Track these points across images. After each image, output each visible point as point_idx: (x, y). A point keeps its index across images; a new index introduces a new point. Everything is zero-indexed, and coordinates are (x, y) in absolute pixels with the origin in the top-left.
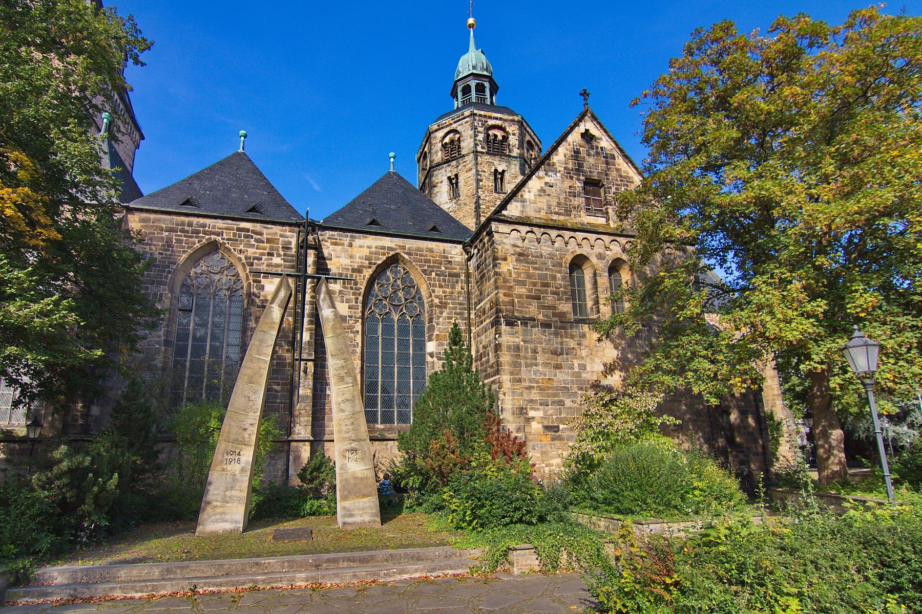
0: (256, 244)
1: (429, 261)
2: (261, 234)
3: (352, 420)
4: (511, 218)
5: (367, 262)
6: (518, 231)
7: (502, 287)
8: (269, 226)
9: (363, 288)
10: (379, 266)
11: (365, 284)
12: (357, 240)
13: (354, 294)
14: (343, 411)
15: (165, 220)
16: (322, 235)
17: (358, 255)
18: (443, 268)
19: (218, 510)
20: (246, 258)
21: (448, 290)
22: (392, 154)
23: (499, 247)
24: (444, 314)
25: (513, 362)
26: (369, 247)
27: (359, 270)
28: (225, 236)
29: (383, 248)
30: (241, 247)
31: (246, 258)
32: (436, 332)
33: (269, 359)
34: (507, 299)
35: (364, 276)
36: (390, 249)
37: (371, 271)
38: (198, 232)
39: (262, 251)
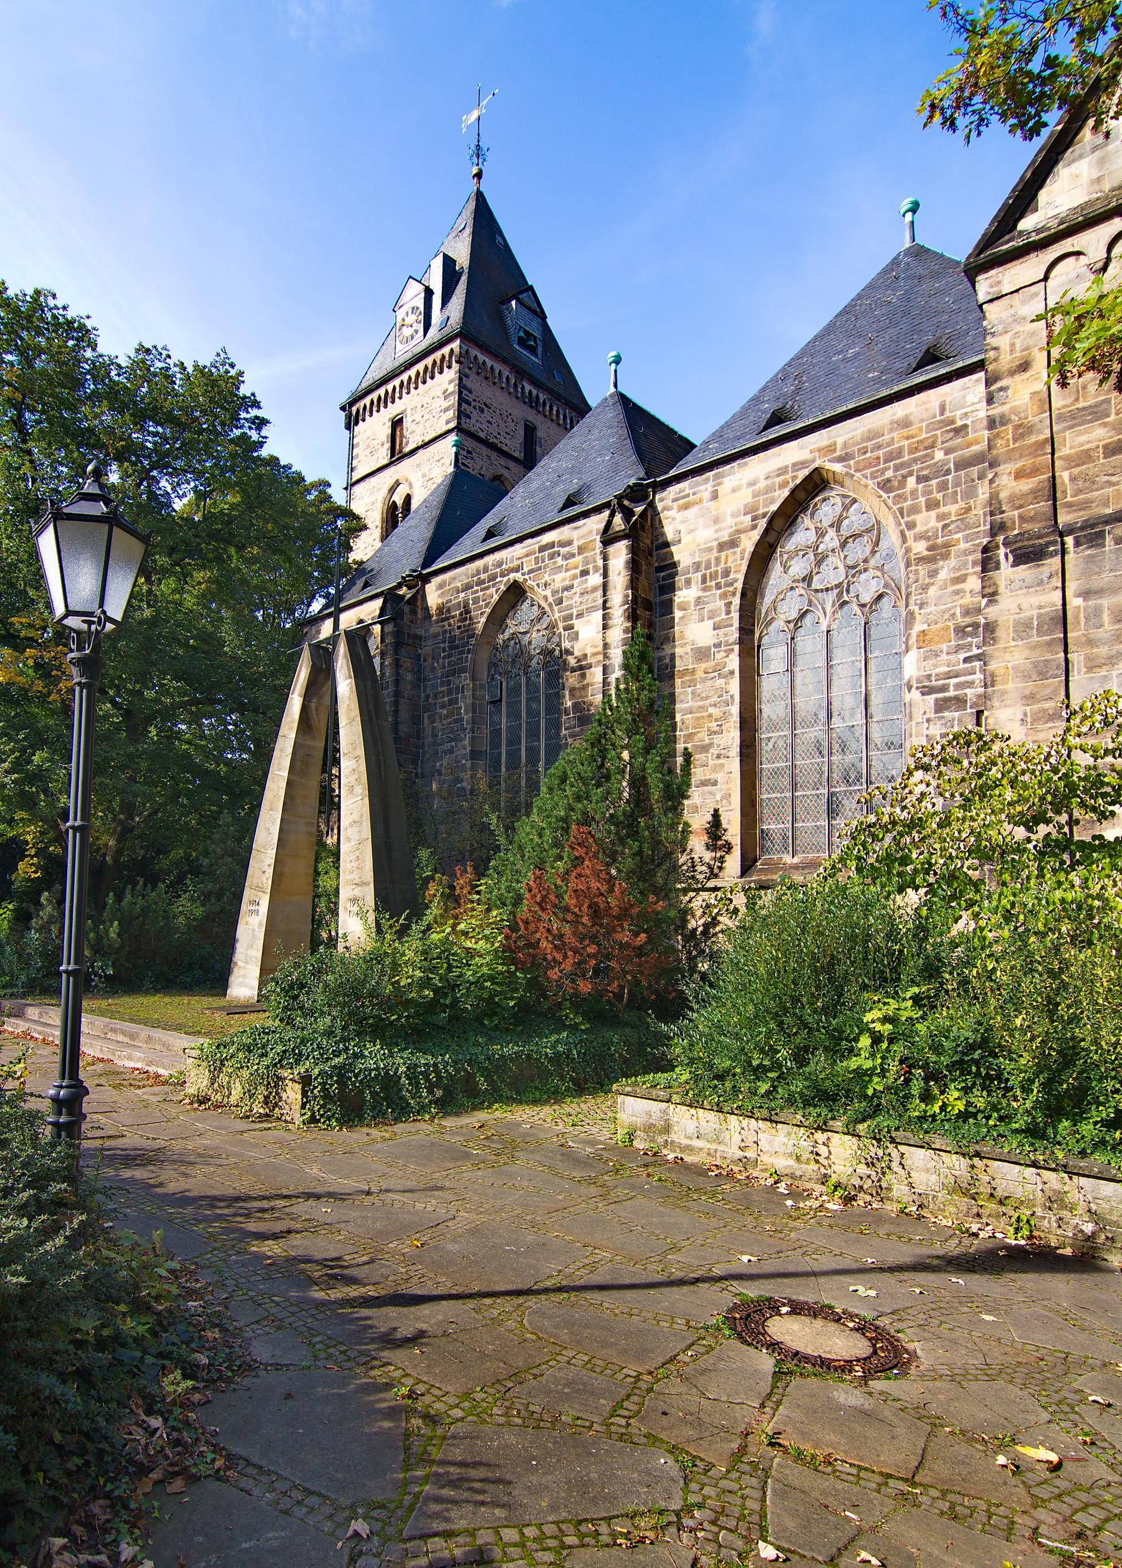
0: (564, 563)
1: (899, 453)
2: (569, 543)
3: (357, 853)
4: (1038, 231)
5: (749, 517)
6: (1078, 254)
7: (1010, 456)
8: (580, 523)
9: (741, 577)
10: (775, 515)
11: (744, 568)
12: (726, 480)
13: (723, 596)
14: (349, 839)
15: (460, 575)
16: (661, 500)
17: (729, 511)
18: (939, 455)
19: (242, 972)
20: (554, 593)
21: (953, 508)
22: (906, 204)
23: (1002, 342)
24: (943, 575)
25: (1035, 665)
26: (751, 484)
27: (733, 543)
28: (526, 569)
29: (783, 471)
30: (547, 578)
31: (554, 593)
32: (918, 627)
33: (286, 774)
34: (1025, 486)
35: (743, 552)
36: (798, 465)
37: (756, 535)
38: (493, 578)
39: (573, 572)
